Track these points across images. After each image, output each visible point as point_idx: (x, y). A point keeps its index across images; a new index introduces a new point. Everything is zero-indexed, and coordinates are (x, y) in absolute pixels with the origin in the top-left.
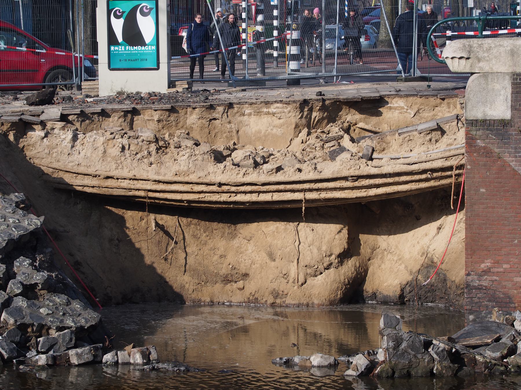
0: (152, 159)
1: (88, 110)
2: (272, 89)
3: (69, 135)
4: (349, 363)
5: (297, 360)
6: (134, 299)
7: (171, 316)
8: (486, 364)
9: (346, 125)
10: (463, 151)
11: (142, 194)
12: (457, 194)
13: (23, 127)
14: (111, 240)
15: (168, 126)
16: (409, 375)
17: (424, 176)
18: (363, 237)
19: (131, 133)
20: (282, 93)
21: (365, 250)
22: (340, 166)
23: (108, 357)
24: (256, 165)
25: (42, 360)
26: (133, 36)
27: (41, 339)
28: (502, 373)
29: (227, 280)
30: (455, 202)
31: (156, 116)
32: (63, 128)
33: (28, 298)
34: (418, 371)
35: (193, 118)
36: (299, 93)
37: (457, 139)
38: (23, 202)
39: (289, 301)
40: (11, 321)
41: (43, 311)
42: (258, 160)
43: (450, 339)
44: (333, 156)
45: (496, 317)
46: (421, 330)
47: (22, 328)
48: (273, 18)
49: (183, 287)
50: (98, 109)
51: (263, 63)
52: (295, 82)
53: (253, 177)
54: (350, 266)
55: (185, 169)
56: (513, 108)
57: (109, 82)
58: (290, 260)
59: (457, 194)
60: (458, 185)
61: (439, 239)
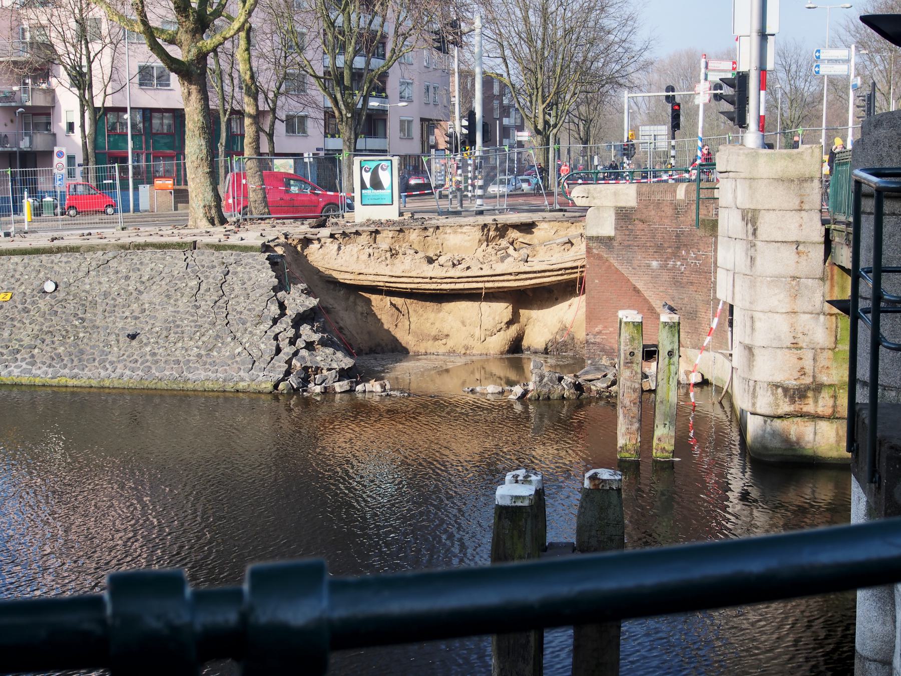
0: (388, 262)
1: (347, 231)
2: (465, 217)
3: (336, 247)
4: (511, 391)
5: (478, 389)
6: (376, 351)
7: (401, 361)
8: (598, 392)
9: (511, 240)
10: (584, 256)
11: (382, 284)
12: (581, 284)
13: (306, 242)
14: (362, 313)
15: (399, 241)
16: (549, 398)
17: (560, 272)
18: (521, 311)
19: (374, 246)
20: (471, 220)
21: (523, 319)
22: (509, 265)
23: (359, 388)
24: (454, 265)
25: (318, 389)
26: (377, 184)
27: (317, 376)
28: (607, 397)
29: (436, 339)
30: (580, 289)
31: (391, 234)
32: (332, 242)
33: (309, 350)
34: (555, 396)
35: (414, 236)
36: (481, 220)
37: (580, 248)
38: (306, 289)
39: (474, 352)
40: (298, 365)
41: (319, 358)
42: (455, 262)
43: (575, 376)
44: (503, 259)
45: (605, 361)
46: (558, 370)
47: (306, 369)
48: (468, 172)
49: (408, 343)
50: (354, 231)
51: (461, 201)
52: (481, 213)
53: (453, 273)
54: (513, 330)
55: (409, 269)
56: (616, 229)
57: (361, 214)
58: (477, 328)
59: (581, 284)
60: (581, 278)
61: (568, 314)
